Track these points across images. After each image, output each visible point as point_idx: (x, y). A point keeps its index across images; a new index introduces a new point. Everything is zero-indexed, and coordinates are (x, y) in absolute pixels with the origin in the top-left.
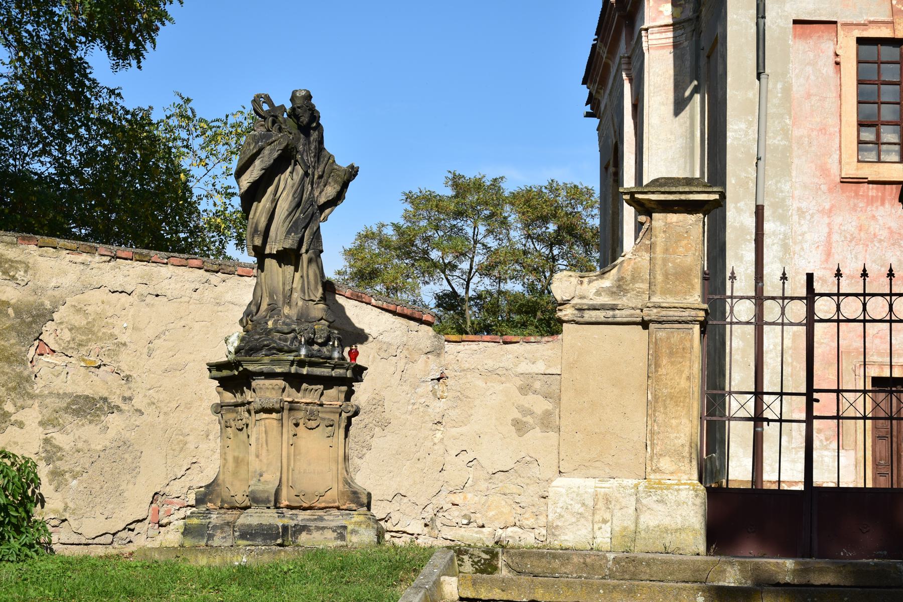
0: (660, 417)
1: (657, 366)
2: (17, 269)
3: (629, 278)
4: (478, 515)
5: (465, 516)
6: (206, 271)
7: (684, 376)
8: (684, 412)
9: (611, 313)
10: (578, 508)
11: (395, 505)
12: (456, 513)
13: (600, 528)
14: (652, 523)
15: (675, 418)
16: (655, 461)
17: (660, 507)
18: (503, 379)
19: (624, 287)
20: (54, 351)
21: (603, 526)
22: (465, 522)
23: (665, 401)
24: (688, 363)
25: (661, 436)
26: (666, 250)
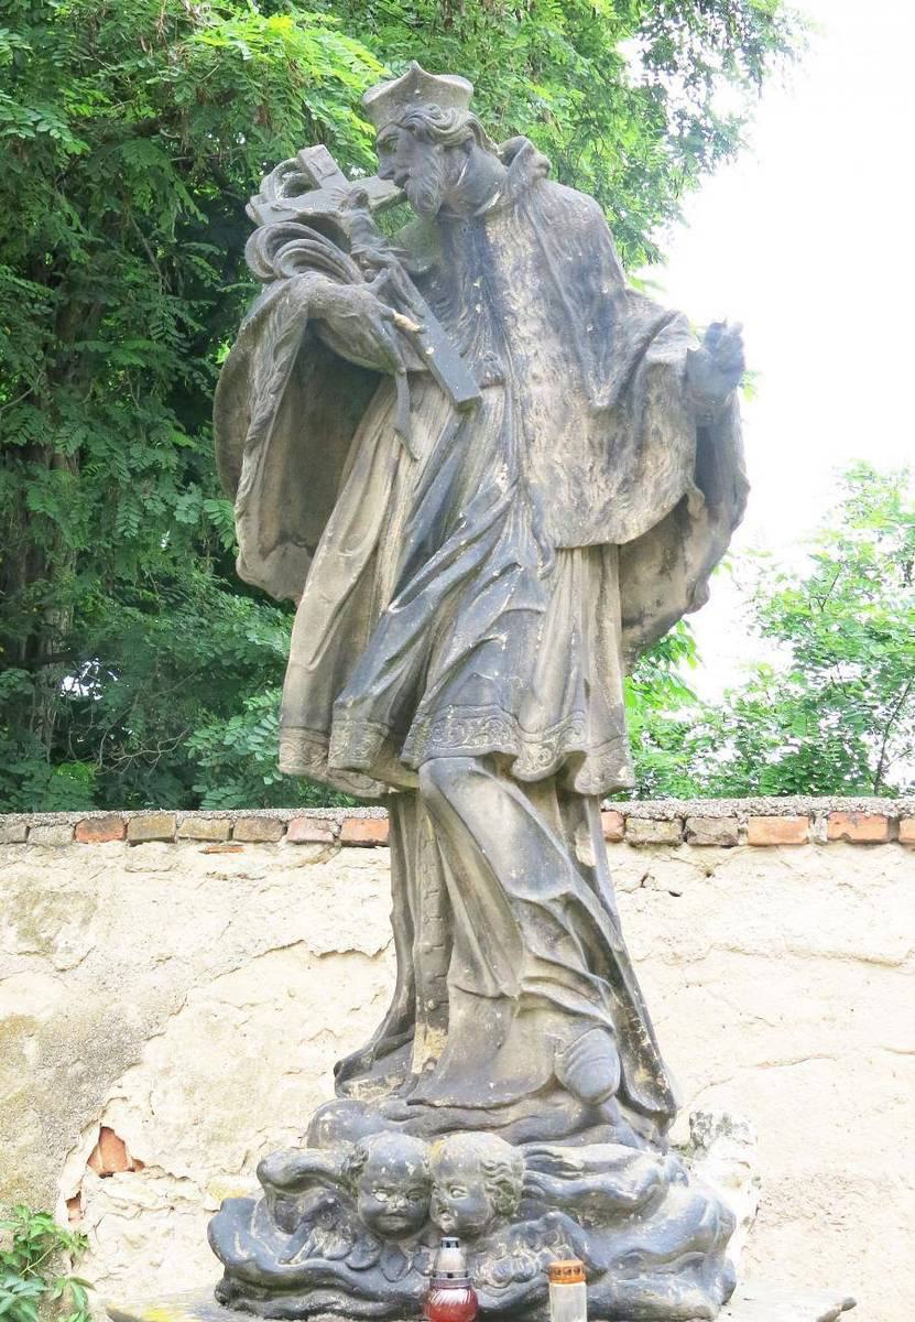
2: (63, 918)
20: (140, 1164)
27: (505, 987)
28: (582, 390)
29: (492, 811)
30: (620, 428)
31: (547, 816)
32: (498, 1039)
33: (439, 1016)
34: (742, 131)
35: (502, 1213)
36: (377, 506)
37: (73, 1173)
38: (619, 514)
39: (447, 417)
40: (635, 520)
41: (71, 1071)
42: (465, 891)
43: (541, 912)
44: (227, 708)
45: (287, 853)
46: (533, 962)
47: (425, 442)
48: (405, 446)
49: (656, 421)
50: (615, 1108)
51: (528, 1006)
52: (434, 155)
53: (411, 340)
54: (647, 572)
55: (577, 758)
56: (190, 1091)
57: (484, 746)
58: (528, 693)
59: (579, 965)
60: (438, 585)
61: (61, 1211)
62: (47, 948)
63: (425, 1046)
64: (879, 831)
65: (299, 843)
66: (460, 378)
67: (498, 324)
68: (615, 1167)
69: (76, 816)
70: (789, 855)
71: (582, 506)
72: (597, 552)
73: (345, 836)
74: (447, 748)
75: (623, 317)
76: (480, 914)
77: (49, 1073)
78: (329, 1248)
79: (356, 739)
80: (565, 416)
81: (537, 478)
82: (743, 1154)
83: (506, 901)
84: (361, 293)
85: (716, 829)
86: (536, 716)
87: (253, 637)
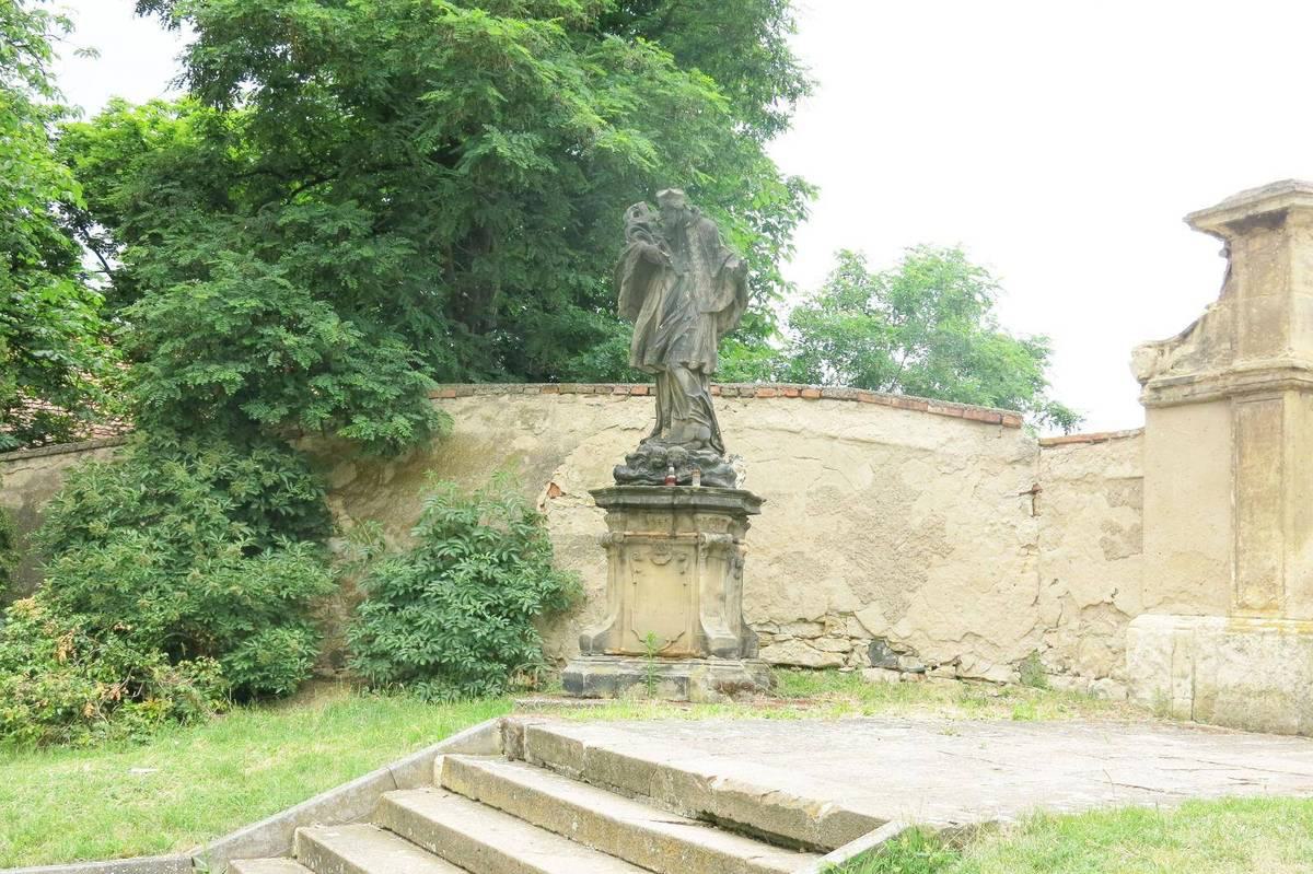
0: (1246, 529)
1: (1242, 455)
2: (537, 418)
3: (1213, 338)
4: (1072, 661)
5: (1059, 661)
6: (724, 397)
7: (1274, 467)
8: (1275, 519)
9: (1187, 390)
10: (1155, 656)
11: (966, 647)
12: (1051, 658)
13: (1179, 685)
14: (1232, 681)
15: (1264, 529)
16: (1240, 591)
17: (1238, 658)
18: (1093, 487)
19: (1209, 351)
20: (564, 494)
21: (1183, 682)
22: (1060, 668)
23: (1251, 505)
24: (1278, 448)
25: (1248, 555)
26: (1249, 292)
27: (685, 417)
28: (710, 273)
29: (683, 376)
30: (718, 283)
31: (697, 378)
32: (683, 430)
33: (668, 425)
34: (789, 121)
35: (683, 463)
36: (656, 301)
37: (542, 497)
38: (717, 303)
39: (675, 279)
40: (721, 306)
41: (541, 466)
42: (676, 393)
43: (694, 399)
44: (574, 352)
45: (613, 398)
46: (691, 411)
47: (669, 285)
48: (664, 285)
49: (727, 281)
50: (709, 445)
51: (690, 421)
52: (674, 214)
53: (667, 259)
54: (724, 319)
55: (704, 364)
56: (581, 471)
57: (681, 360)
58: (693, 349)
59: (701, 412)
60: (672, 322)
61: (538, 509)
62: (531, 428)
63: (664, 433)
64: (796, 393)
65: (618, 394)
66: (678, 269)
67: (688, 254)
68: (709, 455)
69: (541, 385)
70: (769, 400)
71: (708, 302)
72: (711, 314)
73: (633, 392)
74: (674, 360)
75: (719, 255)
76: (680, 400)
77: (532, 467)
78: (643, 471)
79: (651, 357)
80: (704, 279)
81: (697, 295)
82: (741, 463)
83: (686, 397)
84: (655, 246)
85: (748, 392)
86: (694, 354)
87: (592, 325)
